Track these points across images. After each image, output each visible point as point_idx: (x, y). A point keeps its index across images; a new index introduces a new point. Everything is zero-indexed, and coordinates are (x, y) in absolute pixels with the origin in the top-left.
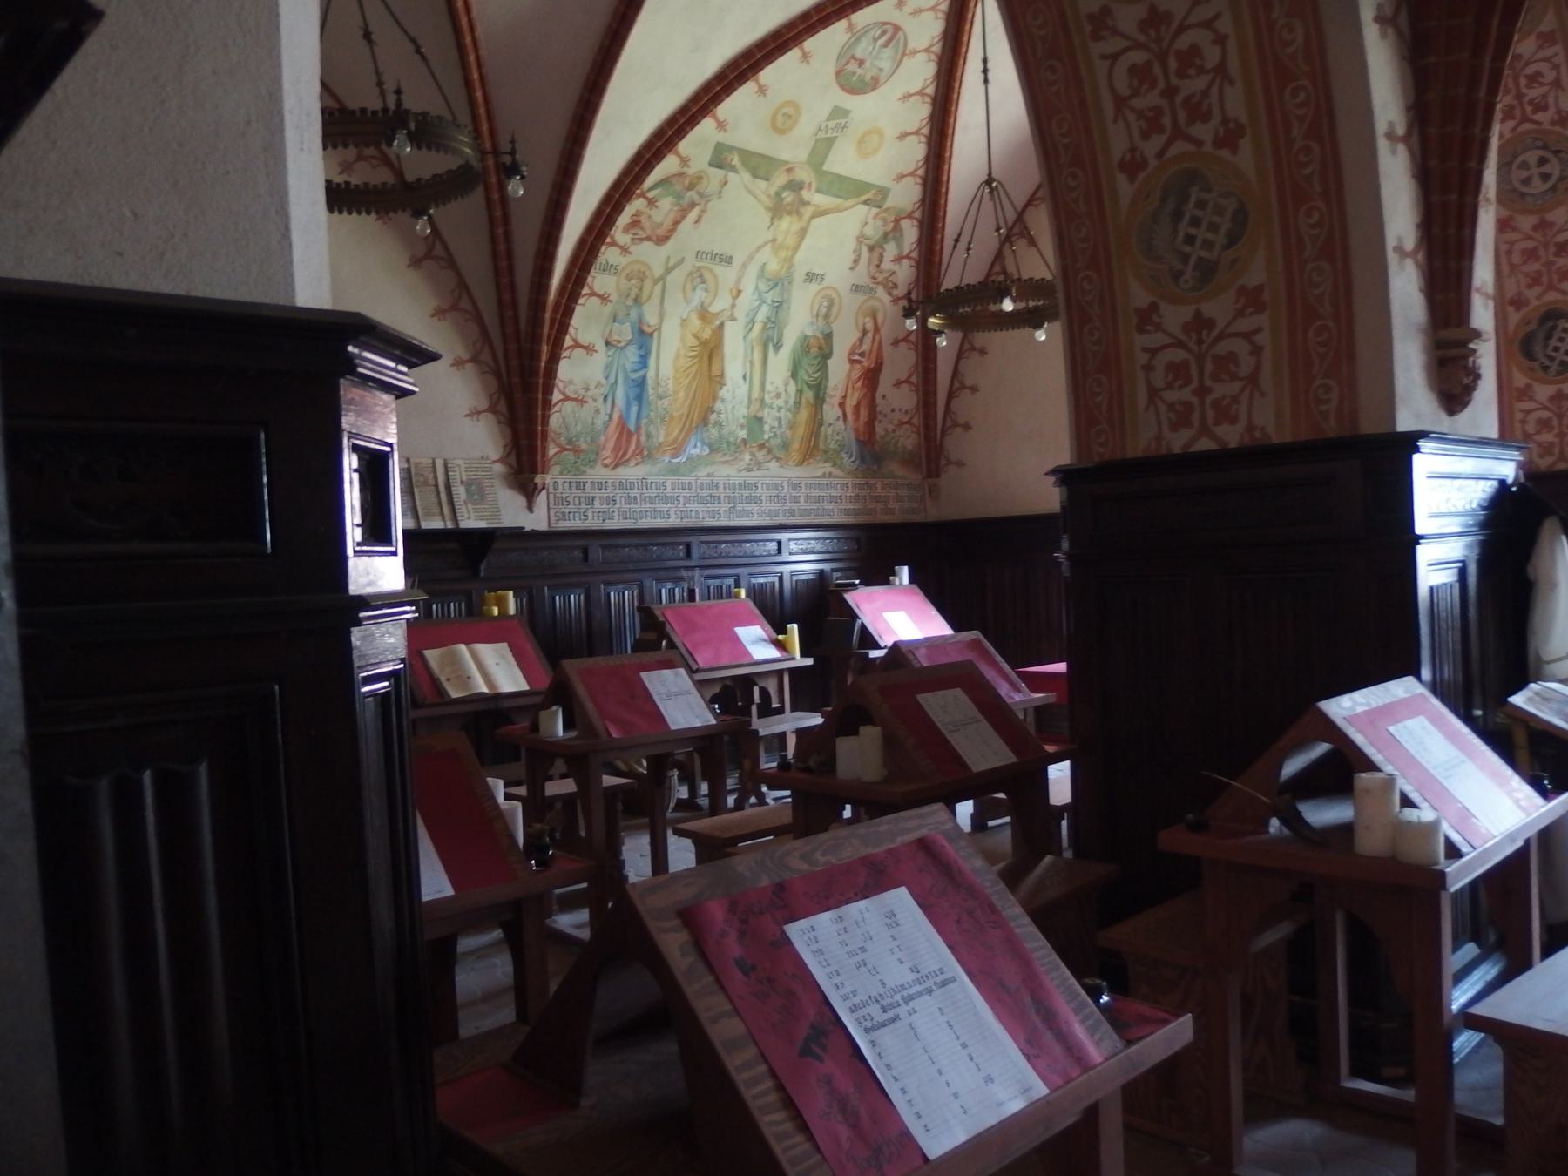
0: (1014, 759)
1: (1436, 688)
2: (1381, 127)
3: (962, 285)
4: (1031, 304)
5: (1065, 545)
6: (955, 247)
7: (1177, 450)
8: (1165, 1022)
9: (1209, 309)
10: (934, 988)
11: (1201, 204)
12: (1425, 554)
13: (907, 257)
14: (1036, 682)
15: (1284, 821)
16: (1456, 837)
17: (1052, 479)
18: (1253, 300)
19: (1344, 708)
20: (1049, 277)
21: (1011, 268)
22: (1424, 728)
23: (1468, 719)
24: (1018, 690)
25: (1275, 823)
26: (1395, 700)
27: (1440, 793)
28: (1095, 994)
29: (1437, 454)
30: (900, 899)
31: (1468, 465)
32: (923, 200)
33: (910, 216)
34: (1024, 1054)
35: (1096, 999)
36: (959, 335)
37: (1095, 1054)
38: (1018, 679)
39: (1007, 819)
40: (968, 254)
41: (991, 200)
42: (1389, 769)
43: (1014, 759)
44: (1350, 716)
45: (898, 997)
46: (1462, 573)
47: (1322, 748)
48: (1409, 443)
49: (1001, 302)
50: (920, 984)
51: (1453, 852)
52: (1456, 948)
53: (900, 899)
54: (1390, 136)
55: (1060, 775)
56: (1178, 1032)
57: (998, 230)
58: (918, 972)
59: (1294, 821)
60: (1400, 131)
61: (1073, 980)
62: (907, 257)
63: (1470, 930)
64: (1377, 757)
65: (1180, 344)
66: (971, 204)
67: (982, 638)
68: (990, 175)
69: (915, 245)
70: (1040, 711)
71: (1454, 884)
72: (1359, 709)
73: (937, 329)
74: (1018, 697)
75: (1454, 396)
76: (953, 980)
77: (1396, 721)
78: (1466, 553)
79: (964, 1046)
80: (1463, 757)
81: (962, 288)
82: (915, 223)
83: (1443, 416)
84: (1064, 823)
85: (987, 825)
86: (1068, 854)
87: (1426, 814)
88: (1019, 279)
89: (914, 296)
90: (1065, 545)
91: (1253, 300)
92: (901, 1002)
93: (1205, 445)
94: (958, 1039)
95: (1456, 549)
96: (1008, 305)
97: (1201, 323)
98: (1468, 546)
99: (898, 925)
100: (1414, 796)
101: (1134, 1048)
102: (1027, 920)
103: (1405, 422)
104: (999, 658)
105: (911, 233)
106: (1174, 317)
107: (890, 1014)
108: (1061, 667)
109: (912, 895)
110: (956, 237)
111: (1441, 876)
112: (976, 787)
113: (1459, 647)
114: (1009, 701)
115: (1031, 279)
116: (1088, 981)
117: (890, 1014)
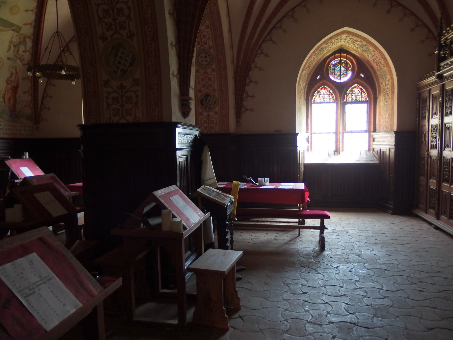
0: (66, 212)
1: (181, 188)
2: (169, 42)
3: (48, 64)
4: (71, 73)
5: (82, 148)
6: (45, 51)
7: (115, 122)
8: (114, 281)
9: (210, 113)
10: (46, 281)
11: (123, 53)
12: (178, 153)
13: (28, 51)
14: (73, 189)
15: (144, 224)
16: (185, 224)
17: (78, 128)
18: (216, 113)
19: (159, 193)
20: (77, 66)
21: (64, 61)
22: (178, 198)
23: (188, 195)
24: (67, 191)
25: (142, 225)
26: (171, 191)
27: (181, 214)
28: (95, 276)
29: (181, 128)
30: (34, 256)
31: (188, 131)
32: (34, 34)
33: (29, 38)
34: (75, 296)
35: (95, 278)
36: (46, 79)
37: (95, 292)
38: (67, 188)
39: (64, 231)
40: (50, 54)
41: (58, 38)
42: (170, 208)
43: (66, 212)
44: (160, 195)
45: (34, 286)
46: (187, 158)
47: (154, 204)
48: (174, 125)
49: (61, 71)
50: (42, 281)
51: (185, 228)
52: (186, 253)
53: (34, 256)
54: (171, 44)
55: (81, 216)
56: (119, 283)
57: (60, 48)
58: (41, 277)
59: (147, 224)
60: (174, 43)
61: (88, 273)
62: (28, 51)
63: (189, 248)
64: (167, 206)
65: (206, 118)
66: (52, 37)
67: (55, 176)
68: (58, 30)
69: (31, 48)
70: (74, 197)
71: (185, 236)
72: (163, 194)
73: (39, 77)
74: (67, 194)
75: (185, 114)
76: (52, 278)
77: (171, 196)
78: (188, 153)
79: (56, 297)
80: (187, 205)
81: (48, 65)
82: (31, 40)
83: (183, 118)
84: (82, 230)
85: (57, 233)
86: (84, 239)
87: (179, 219)
88: (67, 65)
89: (31, 65)
90: (82, 148)
91: (216, 113)
92: (36, 287)
93: (123, 121)
94: (55, 295)
95: (185, 152)
96: (63, 73)
97: (209, 115)
98: (188, 152)
99: (33, 264)
100: (176, 215)
101: (107, 289)
102: (74, 258)
103: (174, 120)
104: (60, 182)
105: (29, 44)
106: (205, 114)
107: (32, 291)
108: (81, 184)
109: (38, 255)
110: (46, 48)
111: (182, 234)
112: (54, 221)
113: (186, 177)
114: (65, 195)
115: (71, 65)
116: (93, 273)
117: (32, 291)
